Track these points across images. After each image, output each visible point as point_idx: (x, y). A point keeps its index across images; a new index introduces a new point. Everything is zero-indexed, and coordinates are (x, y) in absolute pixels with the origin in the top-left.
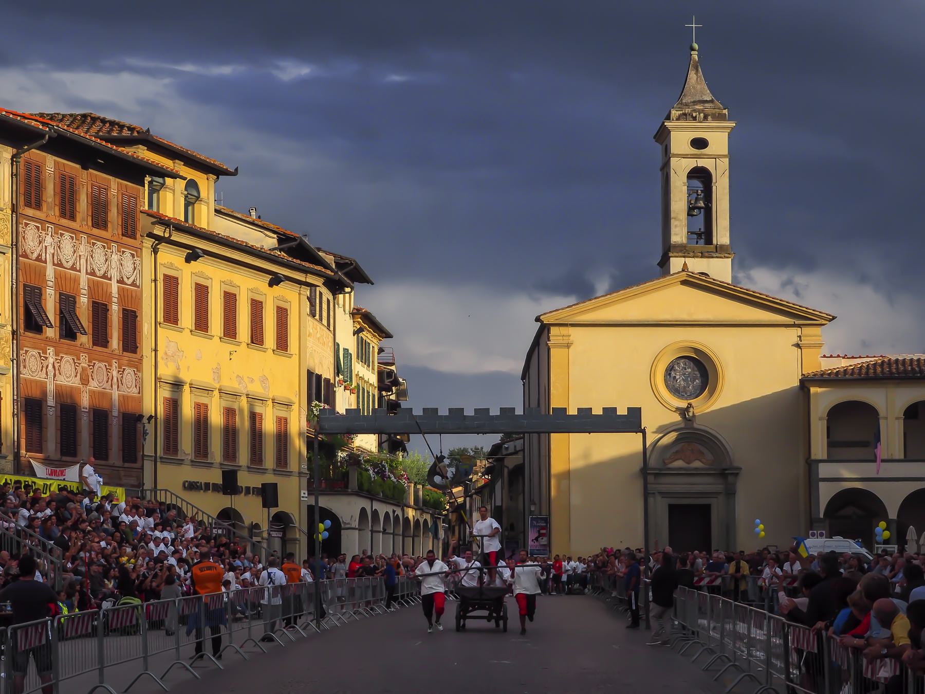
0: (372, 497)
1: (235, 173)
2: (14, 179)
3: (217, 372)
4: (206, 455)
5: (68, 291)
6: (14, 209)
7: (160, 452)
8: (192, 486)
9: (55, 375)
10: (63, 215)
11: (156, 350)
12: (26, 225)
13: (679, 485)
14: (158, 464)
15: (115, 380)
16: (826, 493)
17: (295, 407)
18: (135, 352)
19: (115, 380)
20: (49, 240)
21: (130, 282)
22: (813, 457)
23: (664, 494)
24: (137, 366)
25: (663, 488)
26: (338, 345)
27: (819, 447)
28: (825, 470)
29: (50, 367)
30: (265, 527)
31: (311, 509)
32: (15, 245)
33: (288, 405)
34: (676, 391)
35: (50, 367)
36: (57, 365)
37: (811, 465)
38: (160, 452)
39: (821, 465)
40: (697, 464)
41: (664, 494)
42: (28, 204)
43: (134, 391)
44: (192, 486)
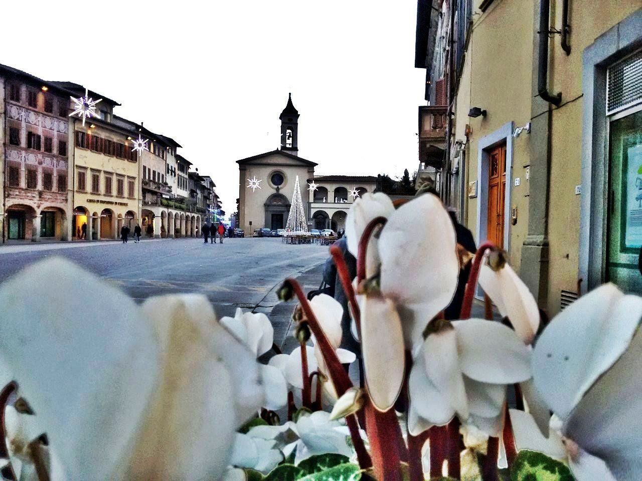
0: (168, 206)
1: (120, 105)
2: (128, 127)
3: (103, 165)
4: (98, 190)
5: (63, 140)
6: (5, 100)
7: (76, 189)
8: (91, 201)
9: (25, 160)
10: (30, 104)
11: (74, 155)
12: (11, 107)
13: (276, 209)
14: (75, 193)
15: (55, 164)
16: (313, 211)
17: (137, 179)
18: (65, 155)
19: (55, 164)
20: (23, 114)
21: (63, 132)
22: (310, 202)
23: (270, 211)
24: (66, 160)
25: (270, 209)
26: (168, 165)
27: (311, 199)
28: (313, 205)
29: (23, 157)
30: (123, 216)
31: (143, 211)
32: (5, 113)
33: (134, 178)
34: (275, 184)
35: (23, 157)
36: (26, 157)
37: (309, 203)
38: (75, 189)
39: (312, 204)
40: (280, 203)
41: (270, 211)
42: (12, 99)
43: (64, 169)
44: (91, 201)
